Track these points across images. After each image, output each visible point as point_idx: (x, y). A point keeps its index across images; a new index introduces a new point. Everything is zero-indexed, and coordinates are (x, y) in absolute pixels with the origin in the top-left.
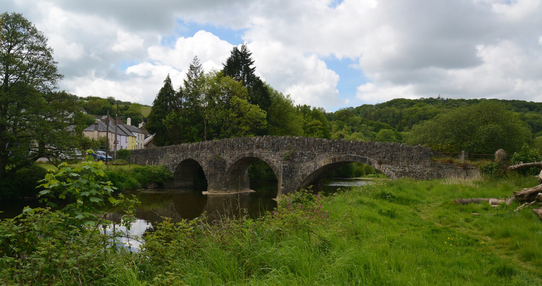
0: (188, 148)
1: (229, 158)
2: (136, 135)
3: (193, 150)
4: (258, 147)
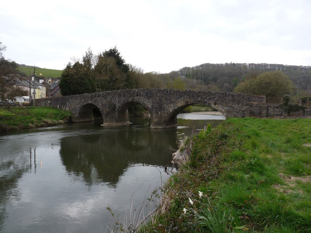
0: (88, 97)
1: (118, 102)
2: (41, 87)
3: (92, 98)
4: (137, 95)
